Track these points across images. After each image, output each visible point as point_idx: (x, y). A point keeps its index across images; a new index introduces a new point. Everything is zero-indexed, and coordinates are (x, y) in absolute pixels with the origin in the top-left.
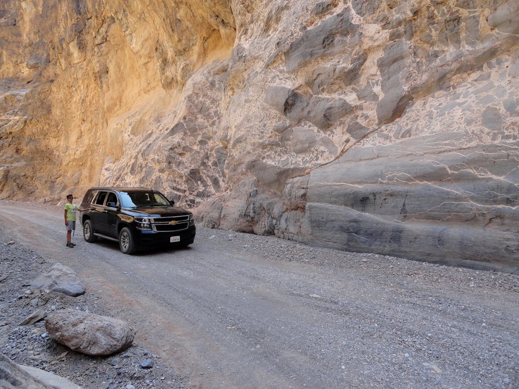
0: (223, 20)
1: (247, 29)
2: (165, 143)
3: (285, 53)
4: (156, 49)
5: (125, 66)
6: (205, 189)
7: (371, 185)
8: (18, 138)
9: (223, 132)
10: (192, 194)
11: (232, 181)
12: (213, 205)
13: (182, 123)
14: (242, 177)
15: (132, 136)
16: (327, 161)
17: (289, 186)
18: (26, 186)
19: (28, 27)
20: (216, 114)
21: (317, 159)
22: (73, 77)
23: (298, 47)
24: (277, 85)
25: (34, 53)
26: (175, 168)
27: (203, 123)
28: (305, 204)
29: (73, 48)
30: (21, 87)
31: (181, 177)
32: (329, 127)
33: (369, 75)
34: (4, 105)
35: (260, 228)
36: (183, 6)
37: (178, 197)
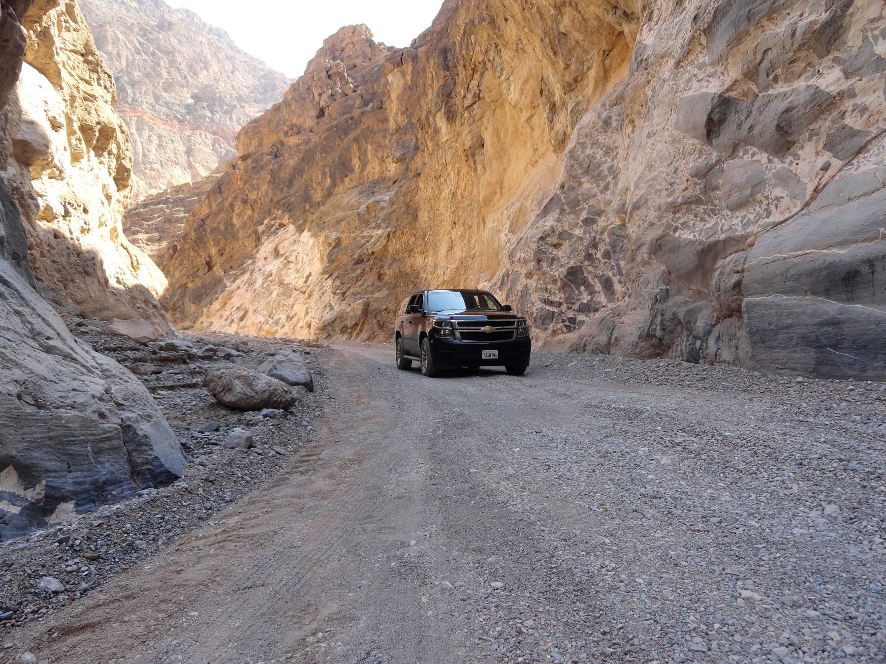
0: (625, 12)
1: (652, 12)
2: (535, 231)
3: (705, 31)
4: (541, 92)
5: (506, 130)
6: (592, 299)
7: (865, 244)
8: (381, 260)
9: (619, 198)
10: (571, 308)
11: (629, 279)
12: (600, 323)
13: (558, 195)
14: (643, 269)
15: (510, 236)
16: (787, 215)
17: (717, 273)
18: (388, 324)
19: (395, 107)
20: (611, 171)
21: (769, 214)
22: (441, 162)
23: (727, 12)
24: (696, 91)
25: (401, 141)
26: (546, 269)
27: (590, 189)
28: (742, 301)
29: (441, 122)
30: (386, 190)
31: (555, 282)
32: (789, 149)
33: (865, 22)
34: (366, 216)
35: (674, 357)
36: (568, 9)
37: (551, 314)
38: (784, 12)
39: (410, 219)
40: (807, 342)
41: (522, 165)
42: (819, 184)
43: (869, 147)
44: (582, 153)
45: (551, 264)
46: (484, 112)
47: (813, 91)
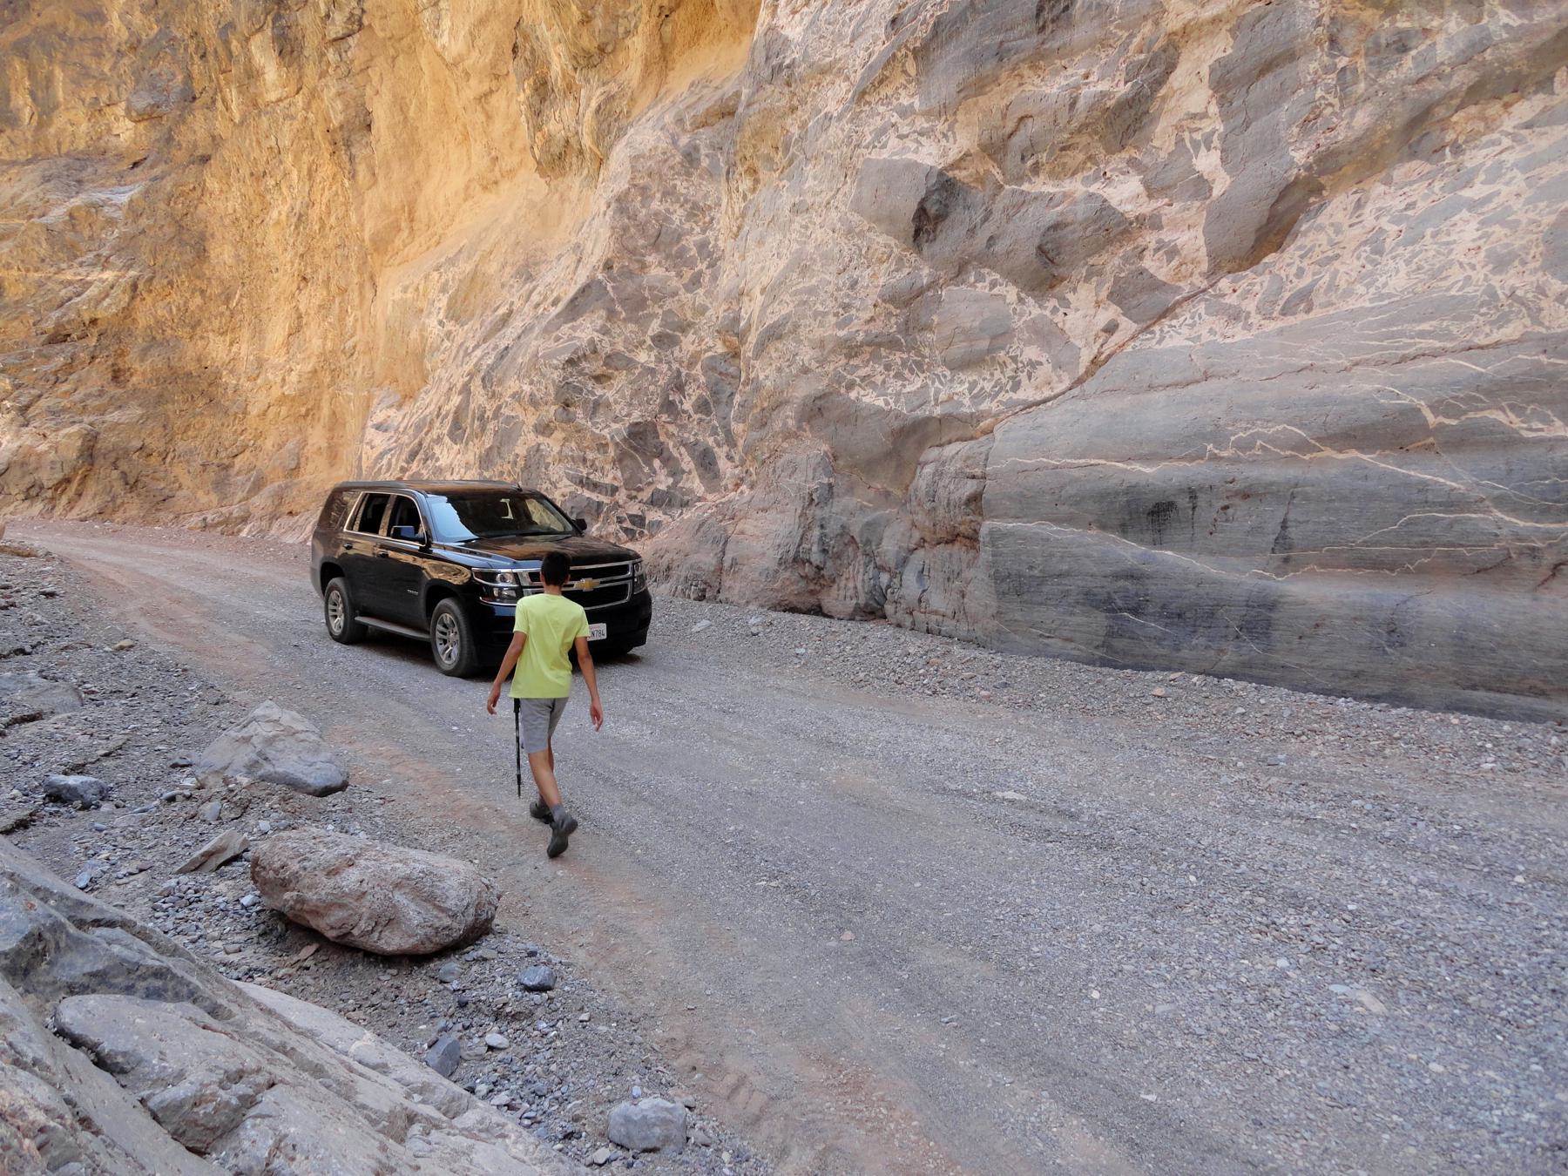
3: (915, 52)
4: (515, 50)
5: (421, 106)
6: (676, 483)
7: (1182, 464)
8: (118, 337)
9: (724, 307)
10: (636, 497)
12: (698, 530)
14: (785, 445)
15: (450, 326)
16: (1047, 393)
17: (929, 469)
21: (1016, 386)
22: (266, 144)
25: (145, 74)
26: (583, 422)
27: (665, 280)
28: (979, 524)
29: (262, 54)
30: (114, 181)
31: (602, 447)
32: (1052, 287)
34: (69, 236)
35: (841, 597)
38: (1058, 62)
39: (189, 257)
40: (1092, 601)
41: (457, 181)
42: (1100, 353)
43: (1178, 310)
44: (643, 206)
45: (594, 413)
46: (372, 58)
47: (1098, 205)
